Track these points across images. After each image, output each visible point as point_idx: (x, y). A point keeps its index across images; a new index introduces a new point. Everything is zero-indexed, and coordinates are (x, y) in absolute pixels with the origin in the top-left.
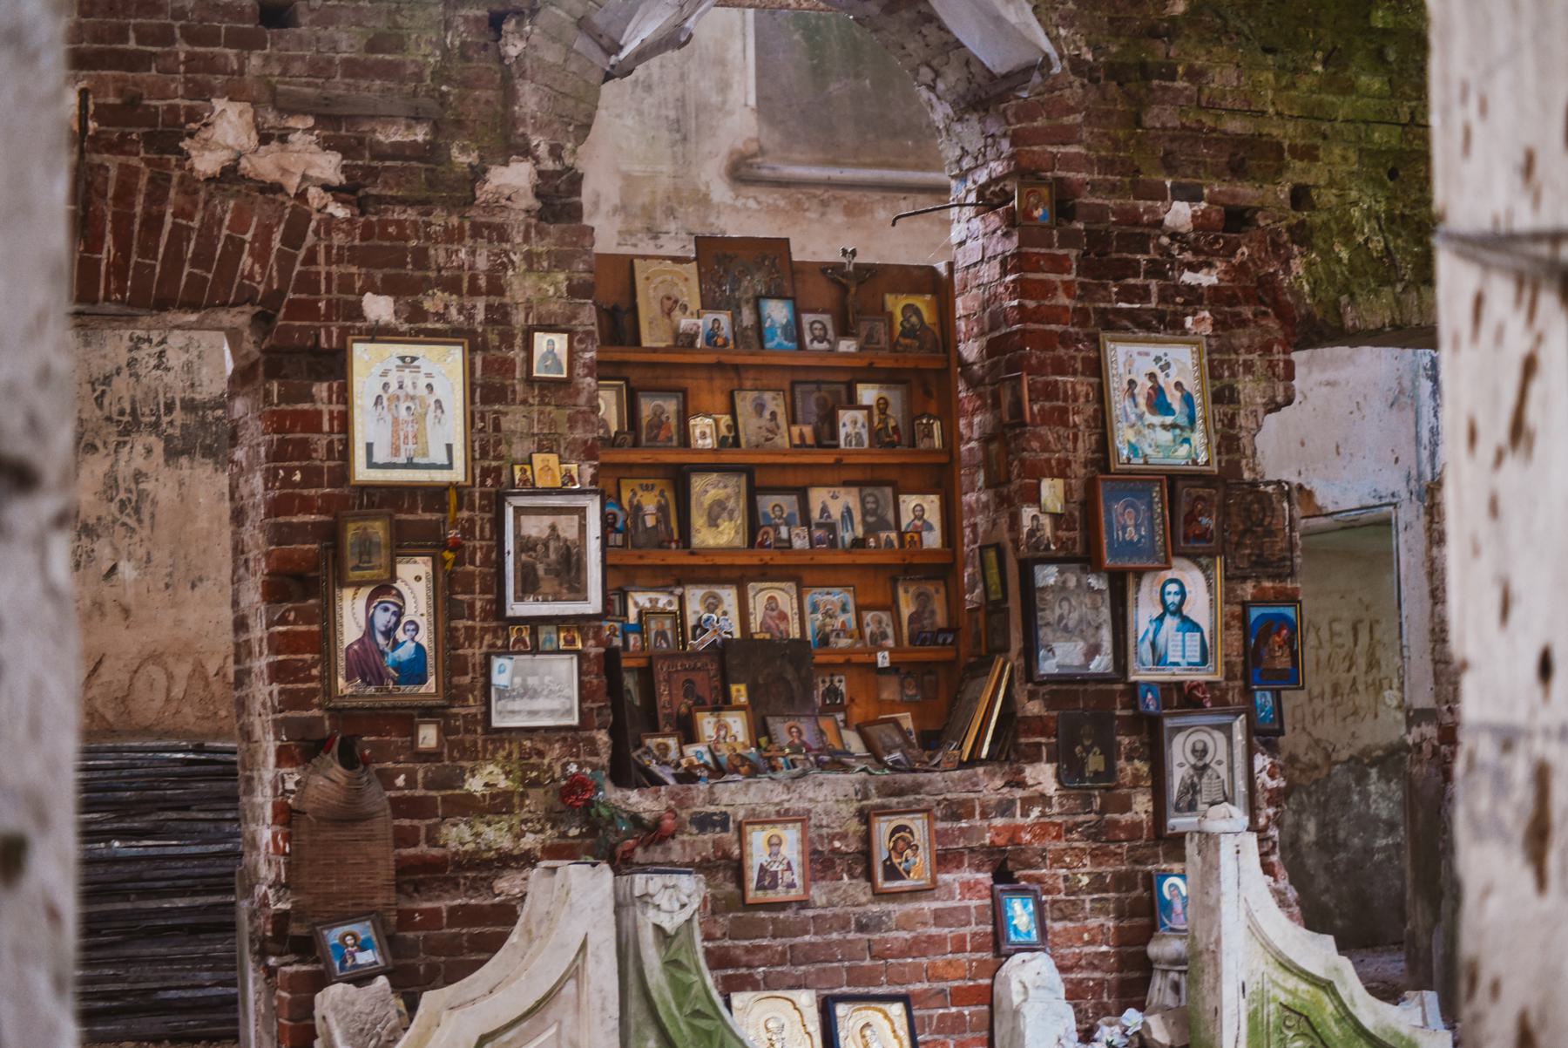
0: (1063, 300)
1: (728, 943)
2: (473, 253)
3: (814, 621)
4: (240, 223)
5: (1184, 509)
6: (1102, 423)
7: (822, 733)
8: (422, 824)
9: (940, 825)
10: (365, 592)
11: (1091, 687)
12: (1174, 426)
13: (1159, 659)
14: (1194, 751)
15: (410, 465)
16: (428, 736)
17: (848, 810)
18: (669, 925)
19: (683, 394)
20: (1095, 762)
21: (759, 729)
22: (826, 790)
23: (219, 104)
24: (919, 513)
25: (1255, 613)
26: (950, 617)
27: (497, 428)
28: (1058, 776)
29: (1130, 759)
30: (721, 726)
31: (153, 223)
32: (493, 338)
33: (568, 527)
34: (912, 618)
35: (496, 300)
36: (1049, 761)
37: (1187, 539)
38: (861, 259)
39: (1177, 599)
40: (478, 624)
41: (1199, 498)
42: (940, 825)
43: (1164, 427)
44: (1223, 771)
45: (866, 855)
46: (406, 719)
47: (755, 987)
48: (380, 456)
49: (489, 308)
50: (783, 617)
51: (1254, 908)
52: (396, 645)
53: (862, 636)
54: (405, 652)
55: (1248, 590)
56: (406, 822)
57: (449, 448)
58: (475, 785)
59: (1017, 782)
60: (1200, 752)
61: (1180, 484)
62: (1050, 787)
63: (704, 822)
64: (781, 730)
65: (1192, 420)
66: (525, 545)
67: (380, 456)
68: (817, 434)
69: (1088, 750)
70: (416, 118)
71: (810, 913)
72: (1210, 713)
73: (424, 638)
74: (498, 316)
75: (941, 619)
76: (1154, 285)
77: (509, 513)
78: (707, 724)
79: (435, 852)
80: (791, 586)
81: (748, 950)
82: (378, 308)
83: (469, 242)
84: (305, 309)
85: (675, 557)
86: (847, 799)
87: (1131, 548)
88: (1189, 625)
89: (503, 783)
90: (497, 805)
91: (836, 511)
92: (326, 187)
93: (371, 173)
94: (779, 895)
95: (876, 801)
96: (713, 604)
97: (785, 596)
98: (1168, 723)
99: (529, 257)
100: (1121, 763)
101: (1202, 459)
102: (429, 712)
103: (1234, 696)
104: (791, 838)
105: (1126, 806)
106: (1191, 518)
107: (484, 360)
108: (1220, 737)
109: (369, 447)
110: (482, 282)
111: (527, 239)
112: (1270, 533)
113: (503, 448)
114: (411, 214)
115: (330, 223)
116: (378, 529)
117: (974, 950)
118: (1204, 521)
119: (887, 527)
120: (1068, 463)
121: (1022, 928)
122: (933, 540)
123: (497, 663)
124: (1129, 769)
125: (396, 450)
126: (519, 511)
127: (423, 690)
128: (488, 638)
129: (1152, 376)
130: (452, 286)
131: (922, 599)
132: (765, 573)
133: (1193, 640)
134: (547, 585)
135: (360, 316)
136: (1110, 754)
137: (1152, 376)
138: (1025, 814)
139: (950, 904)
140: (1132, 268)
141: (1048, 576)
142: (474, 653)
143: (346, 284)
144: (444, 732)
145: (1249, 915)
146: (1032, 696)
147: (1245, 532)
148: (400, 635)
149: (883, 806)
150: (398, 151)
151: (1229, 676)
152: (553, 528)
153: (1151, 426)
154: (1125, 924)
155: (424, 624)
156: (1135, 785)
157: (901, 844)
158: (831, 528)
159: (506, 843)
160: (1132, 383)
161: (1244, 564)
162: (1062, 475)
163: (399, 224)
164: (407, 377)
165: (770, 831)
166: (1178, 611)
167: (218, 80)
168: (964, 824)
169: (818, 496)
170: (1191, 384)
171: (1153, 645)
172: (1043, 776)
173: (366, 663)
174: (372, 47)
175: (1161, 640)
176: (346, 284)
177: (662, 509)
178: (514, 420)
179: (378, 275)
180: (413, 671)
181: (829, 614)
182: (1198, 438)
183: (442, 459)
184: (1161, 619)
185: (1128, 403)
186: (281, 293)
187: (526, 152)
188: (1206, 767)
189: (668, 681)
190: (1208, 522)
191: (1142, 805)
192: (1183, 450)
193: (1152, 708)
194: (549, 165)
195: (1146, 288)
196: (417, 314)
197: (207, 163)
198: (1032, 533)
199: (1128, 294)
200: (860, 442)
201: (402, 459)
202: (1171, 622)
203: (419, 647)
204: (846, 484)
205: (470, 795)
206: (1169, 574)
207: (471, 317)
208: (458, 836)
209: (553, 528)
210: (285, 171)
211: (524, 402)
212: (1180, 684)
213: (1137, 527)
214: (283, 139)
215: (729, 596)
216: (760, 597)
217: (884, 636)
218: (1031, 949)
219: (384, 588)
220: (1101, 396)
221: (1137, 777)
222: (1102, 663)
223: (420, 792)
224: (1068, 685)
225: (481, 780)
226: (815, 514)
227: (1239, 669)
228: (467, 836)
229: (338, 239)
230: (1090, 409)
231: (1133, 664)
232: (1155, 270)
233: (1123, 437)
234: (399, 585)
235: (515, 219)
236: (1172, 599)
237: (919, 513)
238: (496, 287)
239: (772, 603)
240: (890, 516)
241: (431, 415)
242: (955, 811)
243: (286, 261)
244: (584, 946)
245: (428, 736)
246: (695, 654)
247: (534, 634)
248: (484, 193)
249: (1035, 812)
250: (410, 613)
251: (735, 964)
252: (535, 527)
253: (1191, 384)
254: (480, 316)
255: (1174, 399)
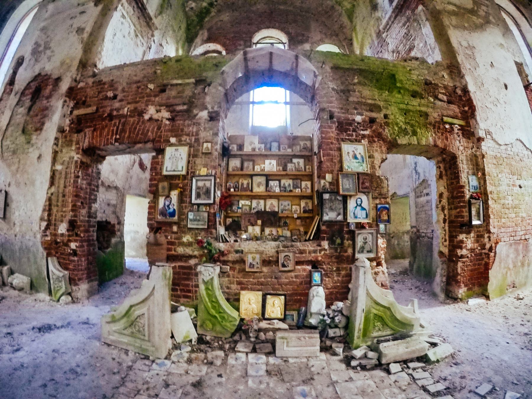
0: (332, 135)
1: (242, 279)
2: (193, 128)
3: (281, 207)
4: (150, 127)
5: (361, 181)
6: (341, 162)
7: (278, 231)
8: (173, 247)
9: (297, 255)
10: (164, 198)
11: (338, 223)
12: (359, 162)
13: (356, 217)
14: (364, 239)
15: (174, 171)
16: (175, 228)
17: (273, 250)
18: (206, 280)
19: (254, 161)
20: (338, 241)
21: (262, 230)
22: (269, 246)
23: (150, 107)
24: (306, 185)
25: (379, 206)
26: (313, 207)
27: (195, 163)
28: (329, 244)
29: (348, 240)
30: (253, 229)
31: (135, 128)
32: (196, 145)
33: (208, 184)
34: (304, 207)
35: (197, 137)
36: (327, 240)
37: (362, 188)
38: (294, 135)
39: (360, 203)
40: (187, 205)
41: (365, 179)
42: (297, 255)
43: (356, 162)
44: (371, 243)
45: (277, 261)
46: (171, 224)
47: (248, 289)
48: (168, 169)
49: (195, 139)
50: (274, 207)
51: (368, 288)
52: (169, 208)
53: (292, 211)
54: (171, 210)
55: (377, 201)
56: (170, 246)
57: (182, 167)
58: (185, 240)
59: (320, 245)
60: (365, 239)
61: (360, 175)
62: (327, 247)
63: (237, 252)
64: (267, 231)
65: (363, 161)
66: (198, 188)
67: (168, 169)
68: (283, 168)
69: (337, 238)
70: (184, 104)
71: (263, 274)
72: (368, 230)
73: (175, 207)
74: (197, 140)
75: (311, 208)
76: (354, 134)
77: (194, 181)
78: (250, 228)
79: (176, 253)
80: (276, 200)
81: (247, 281)
82: (173, 140)
83: (192, 126)
84: (159, 141)
85: (249, 193)
86: (274, 248)
87: (348, 190)
88: (363, 209)
89: (191, 240)
90: (190, 244)
91: (287, 185)
92: (167, 119)
93: (176, 116)
94: (255, 270)
95: (282, 249)
96: (258, 204)
97: (274, 202)
98: (357, 232)
99: (205, 128)
100: (345, 241)
101: (366, 170)
102: (175, 223)
103: (374, 225)
104: (258, 256)
105: (346, 251)
106: (363, 183)
107: (193, 150)
108: (370, 236)
109: (167, 168)
110: (194, 134)
111: (204, 125)
112: (383, 187)
113: (196, 167)
114: (181, 122)
115: (166, 125)
116: (166, 184)
117: (305, 284)
118: (366, 184)
119: (298, 188)
120: (333, 171)
121: (317, 280)
122: (309, 191)
123: (190, 213)
124: (347, 243)
125: (172, 168)
126: (197, 181)
127: (174, 218)
128: (189, 208)
129: (353, 151)
130: (188, 135)
131: (307, 203)
132: (271, 197)
133: (364, 212)
134: (203, 196)
135: (170, 142)
136: (342, 239)
137: (353, 151)
138: (320, 253)
139: (299, 273)
140: (349, 130)
141: (326, 196)
142: (186, 211)
143: (167, 136)
144: (179, 227)
145: (367, 290)
146: (323, 225)
147: (376, 188)
148: (170, 207)
149: (283, 250)
150: (181, 111)
151: (373, 221)
152: (205, 184)
153: (353, 162)
154: (343, 285)
155: (175, 204)
156: (349, 247)
157: (286, 260)
158: (285, 188)
159: (191, 253)
160: (348, 153)
161: (376, 195)
162: (332, 173)
163: (179, 124)
164: (176, 153)
165: (253, 255)
166: (360, 205)
167: (150, 103)
168: (304, 255)
169: (283, 182)
170: (363, 154)
171: (354, 213)
172: (325, 244)
173: (163, 213)
174: (178, 93)
175: (356, 213)
176: (167, 136)
177: (248, 184)
178: (198, 161)
179: (173, 134)
180: (172, 214)
181: (285, 206)
182: (364, 165)
183: (180, 169)
184: (356, 207)
185: (347, 157)
186: (155, 139)
187: (206, 108)
188: (366, 242)
189: (245, 219)
190: (367, 184)
191: (350, 251)
192: (361, 168)
193: (353, 229)
194: (211, 110)
195: (352, 134)
196: (180, 141)
197: (146, 117)
198: (323, 186)
199: (349, 135)
200: (292, 170)
201: (173, 170)
202: (359, 208)
203: (174, 210)
204: (290, 179)
205: (184, 242)
206: (358, 197)
207: (191, 141)
208: (181, 250)
209: (205, 184)
210: (159, 117)
211: (201, 157)
212: (360, 223)
213: (349, 185)
214: (160, 111)
215: (262, 202)
216: (269, 202)
217: (297, 211)
218: (318, 286)
219: (168, 196)
220: (341, 156)
221: (349, 245)
222: (340, 218)
223: (173, 240)
224: (331, 224)
225: (187, 238)
226: (282, 185)
227: (375, 219)
228: (182, 250)
229: (167, 128)
230: (339, 159)
231: (349, 218)
232: (354, 130)
233: (345, 166)
234: (171, 196)
235: (202, 121)
236: (359, 203)
237: (306, 185)
238: (197, 134)
239: (272, 204)
240: (299, 186)
241: (180, 160)
242: (302, 252)
243: (157, 133)
244: (154, 288)
245: (175, 228)
246: (252, 214)
247: (198, 207)
248: (197, 117)
249: (323, 253)
250: (173, 202)
251: (244, 284)
252: (200, 184)
253: (363, 154)
254: (193, 140)
255: (359, 156)
